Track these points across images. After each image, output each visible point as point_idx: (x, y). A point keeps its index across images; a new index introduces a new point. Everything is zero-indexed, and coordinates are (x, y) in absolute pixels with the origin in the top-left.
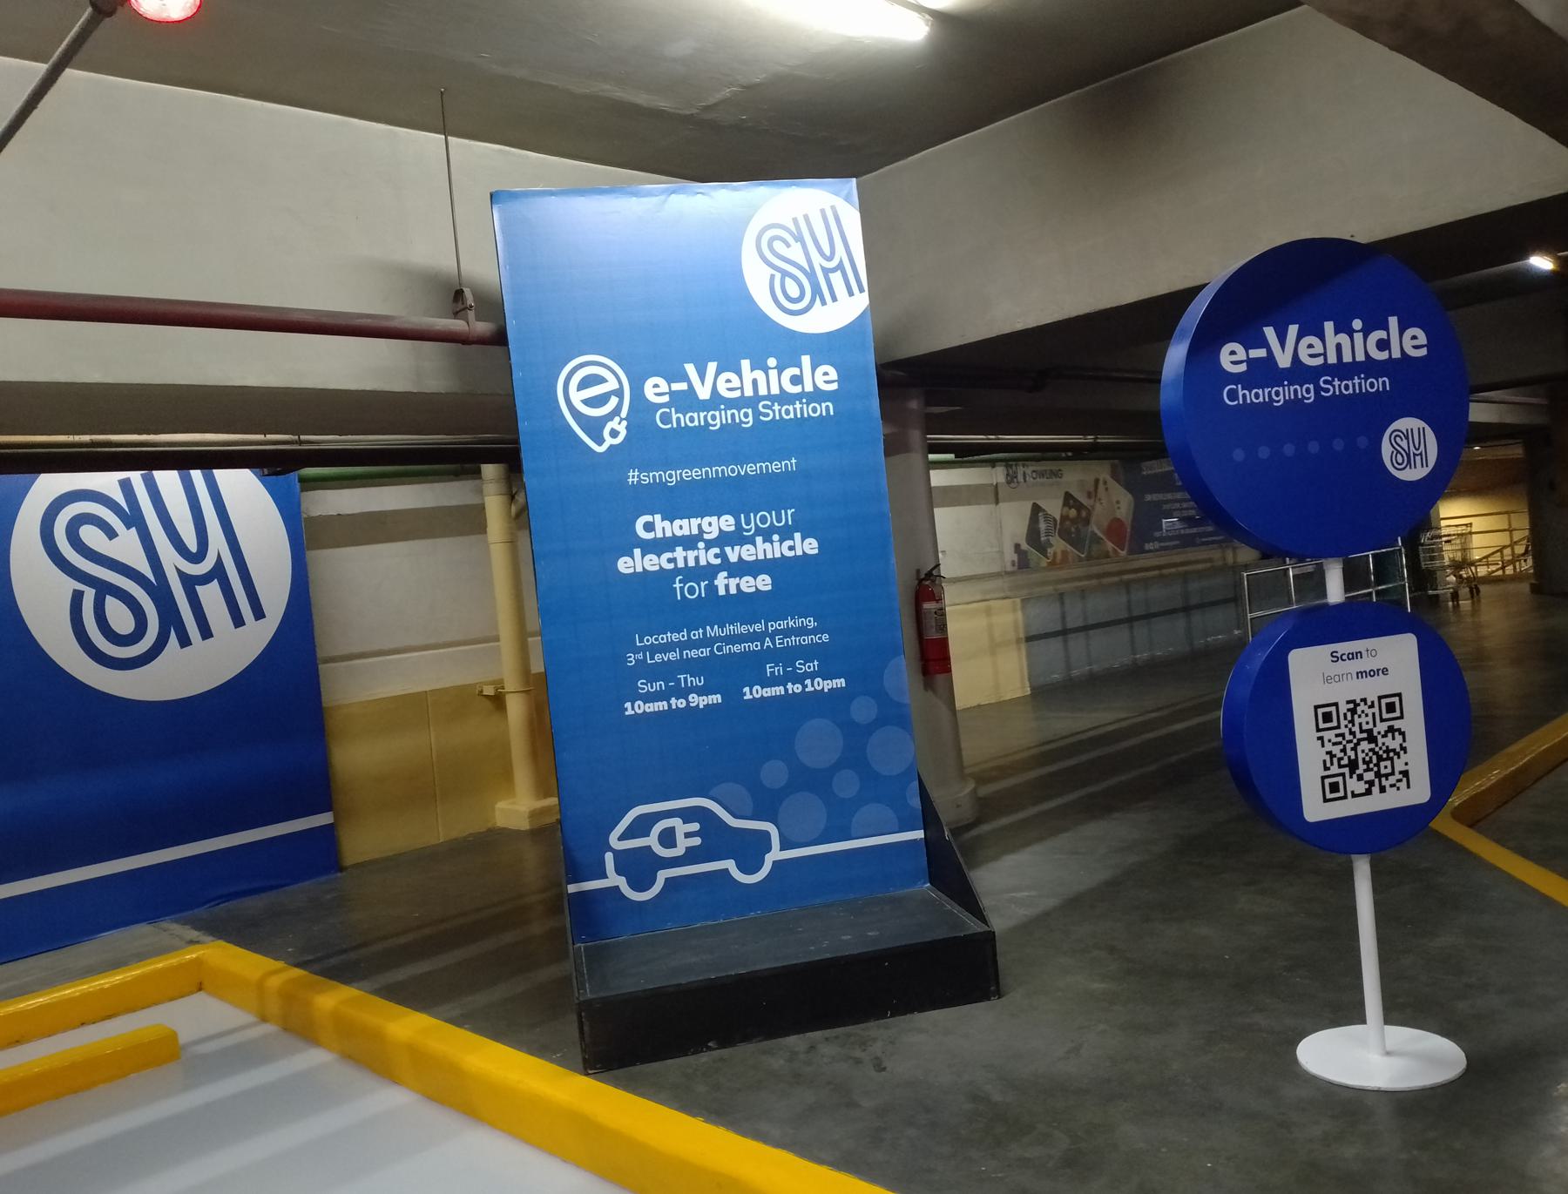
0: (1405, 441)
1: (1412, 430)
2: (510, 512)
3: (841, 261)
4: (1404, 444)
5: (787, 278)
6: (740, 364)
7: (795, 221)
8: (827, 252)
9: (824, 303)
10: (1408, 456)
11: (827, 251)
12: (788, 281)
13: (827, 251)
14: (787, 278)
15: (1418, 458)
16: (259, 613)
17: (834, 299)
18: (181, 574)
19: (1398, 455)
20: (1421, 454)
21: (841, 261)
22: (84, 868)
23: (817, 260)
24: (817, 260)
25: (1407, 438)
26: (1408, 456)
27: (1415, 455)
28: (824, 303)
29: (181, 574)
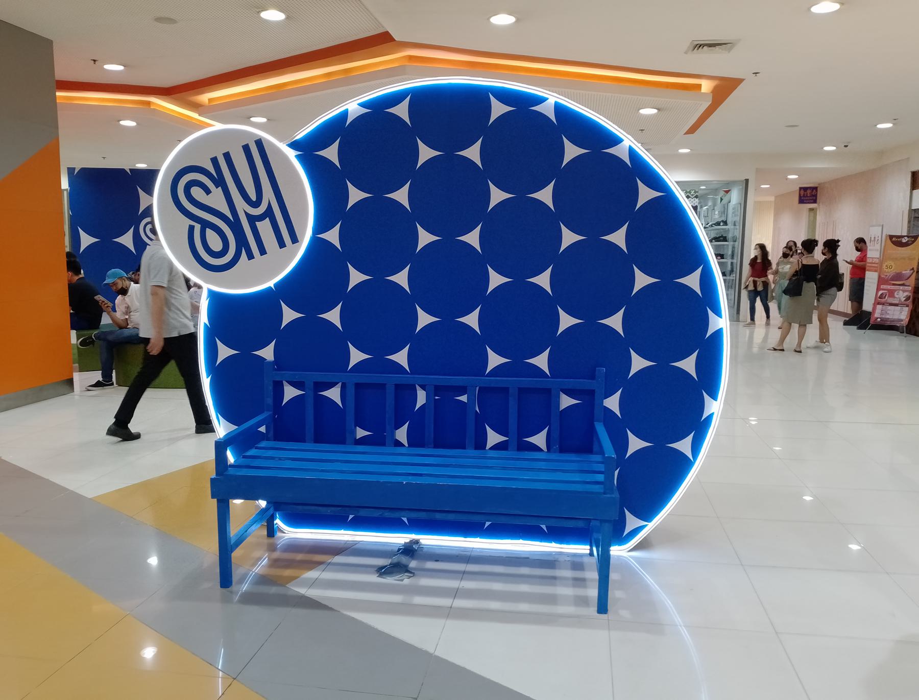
0: (217, 192)
1: (227, 156)
2: (746, 283)
3: (270, 206)
4: (216, 199)
5: (208, 230)
6: (865, 311)
7: (215, 161)
8: (253, 197)
9: (250, 256)
10: (236, 226)
11: (253, 195)
12: (210, 233)
13: (253, 195)
14: (208, 230)
15: (265, 227)
16: (295, 240)
17: (263, 251)
18: (246, 214)
19: (209, 232)
20: (269, 213)
21: (270, 206)
22: (488, 677)
23: (241, 206)
24: (241, 206)
25: (220, 182)
26: (236, 226)
27: (252, 220)
28: (250, 256)
29: (246, 214)
